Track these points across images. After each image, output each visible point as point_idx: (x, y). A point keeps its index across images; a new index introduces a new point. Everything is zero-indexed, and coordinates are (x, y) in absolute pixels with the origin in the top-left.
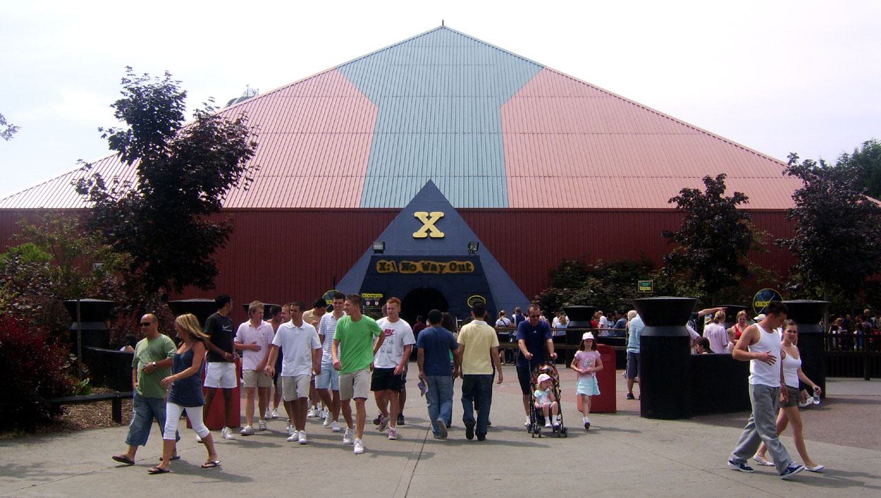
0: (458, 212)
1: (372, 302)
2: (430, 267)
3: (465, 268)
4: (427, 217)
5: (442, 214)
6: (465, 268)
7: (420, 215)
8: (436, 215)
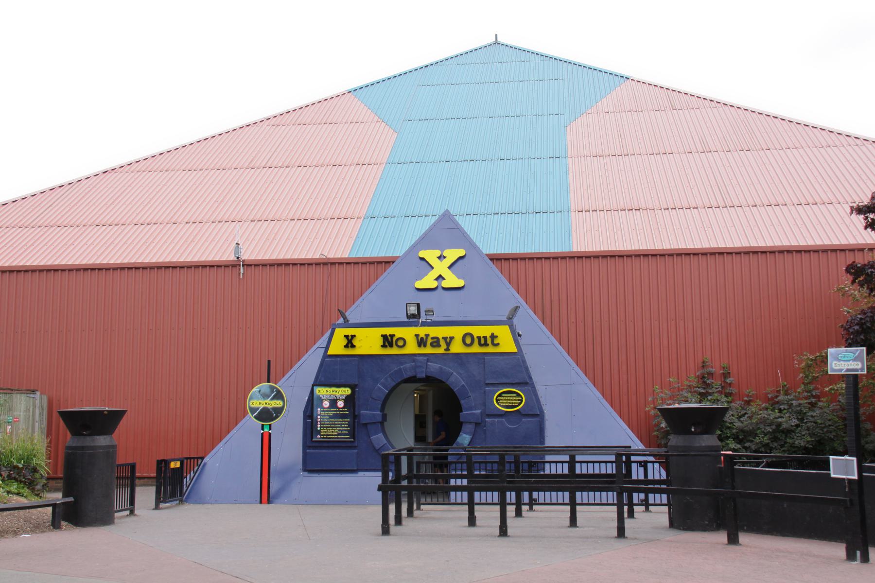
0: (492, 260)
1: (334, 402)
2: (429, 341)
3: (489, 341)
4: (439, 258)
5: (462, 252)
6: (489, 341)
7: (431, 255)
8: (452, 254)
